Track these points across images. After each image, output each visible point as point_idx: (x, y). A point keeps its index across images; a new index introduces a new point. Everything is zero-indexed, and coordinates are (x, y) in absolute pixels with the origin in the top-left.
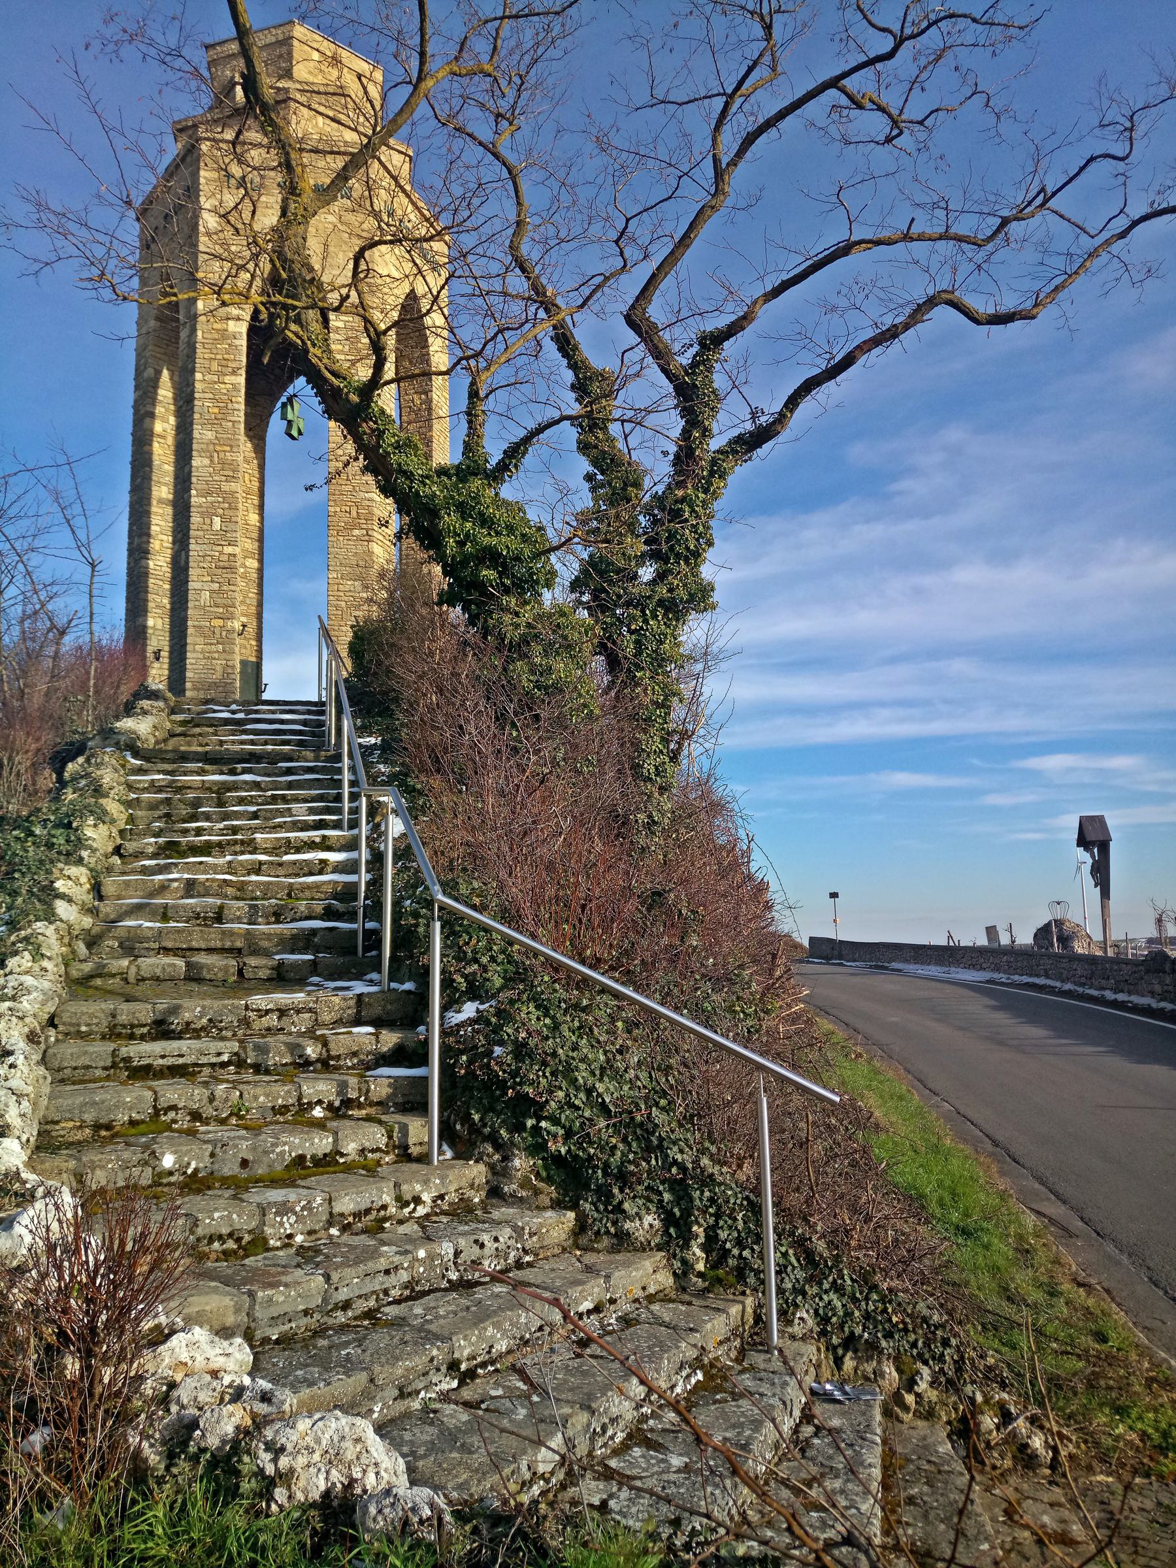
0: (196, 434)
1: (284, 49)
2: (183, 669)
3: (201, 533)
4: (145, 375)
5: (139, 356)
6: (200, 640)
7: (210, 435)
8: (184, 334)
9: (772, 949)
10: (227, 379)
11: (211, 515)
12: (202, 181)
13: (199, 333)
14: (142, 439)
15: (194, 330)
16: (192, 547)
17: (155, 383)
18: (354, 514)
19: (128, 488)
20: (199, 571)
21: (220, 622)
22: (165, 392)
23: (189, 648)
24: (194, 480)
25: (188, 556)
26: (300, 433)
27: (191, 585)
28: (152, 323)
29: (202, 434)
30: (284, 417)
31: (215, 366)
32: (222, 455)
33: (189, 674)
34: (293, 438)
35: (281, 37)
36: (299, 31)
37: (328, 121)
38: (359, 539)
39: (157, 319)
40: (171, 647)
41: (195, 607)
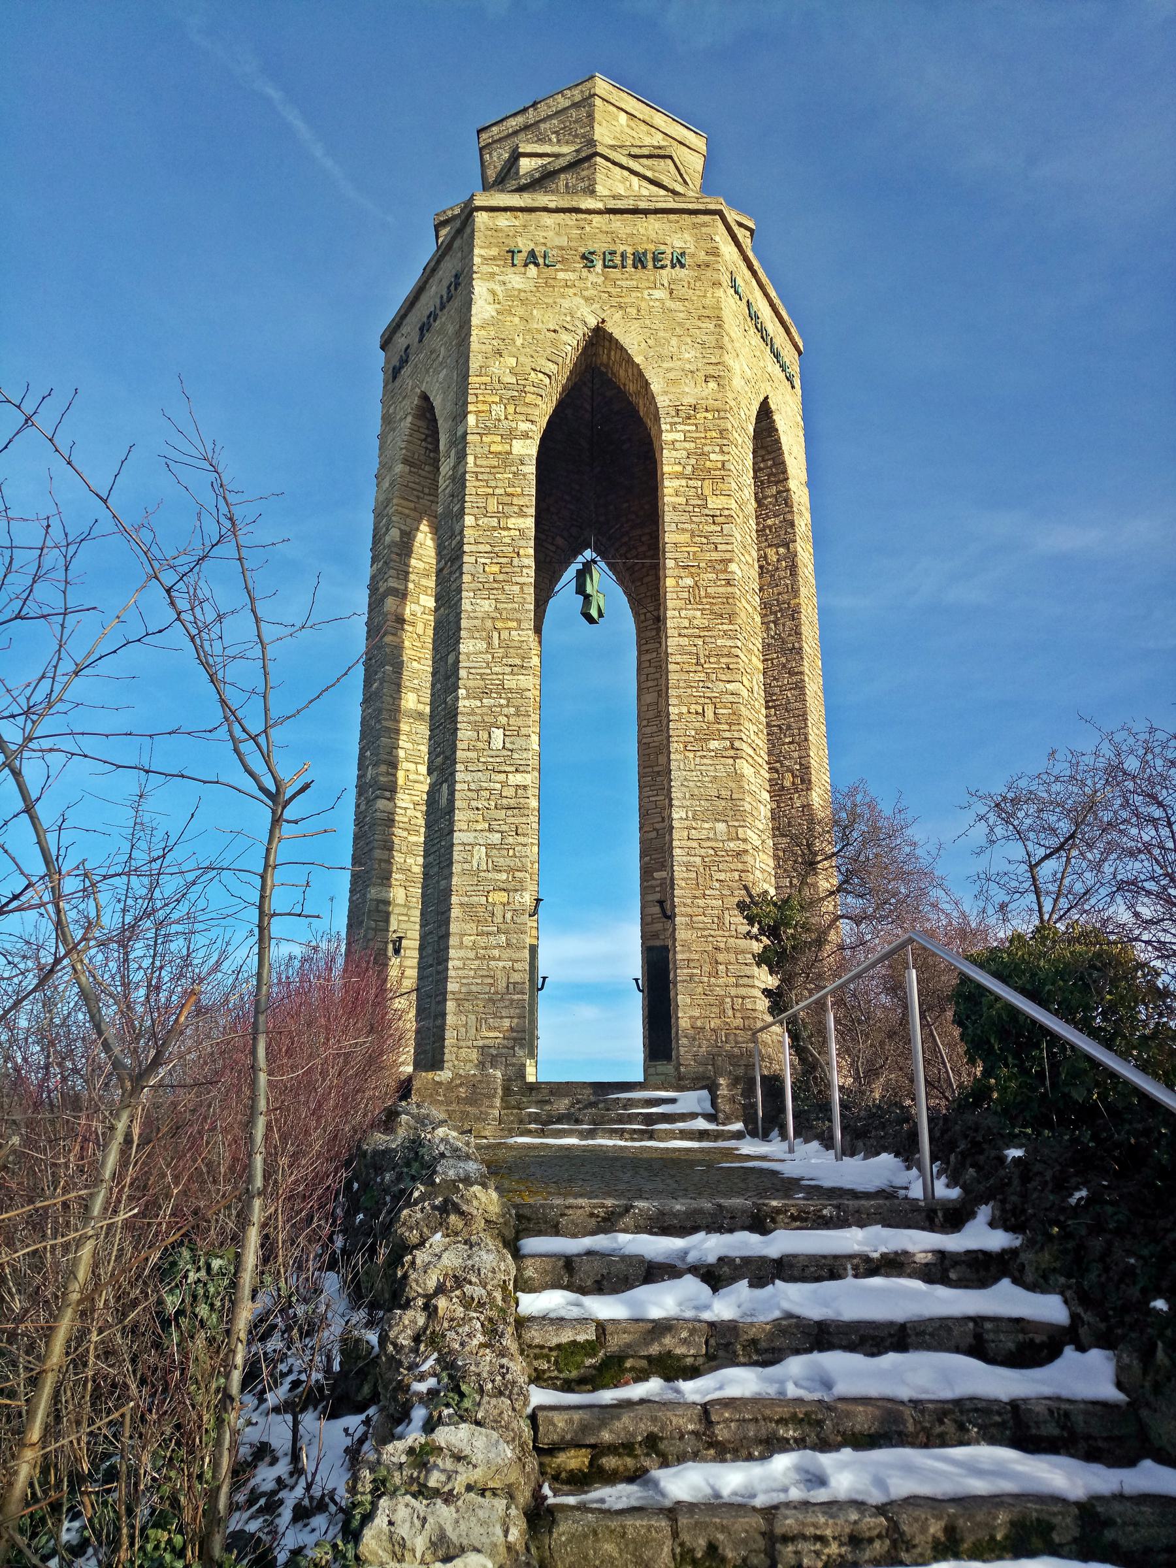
0: (466, 605)
1: (583, 112)
2: (442, 978)
3: (473, 755)
4: (388, 539)
5: (379, 514)
6: (471, 927)
7: (486, 606)
8: (445, 468)
9: (1062, 1293)
10: (511, 522)
11: (489, 727)
12: (477, 260)
13: (470, 459)
14: (384, 627)
15: (462, 456)
16: (459, 776)
17: (405, 547)
18: (710, 715)
19: (360, 698)
20: (471, 815)
21: (502, 897)
22: (425, 541)
23: (453, 941)
24: (463, 673)
25: (452, 792)
26: (601, 615)
27: (458, 837)
28: (399, 468)
29: (475, 605)
30: (581, 589)
31: (493, 505)
32: (504, 635)
33: (452, 986)
34: (591, 620)
35: (578, 98)
36: (602, 86)
37: (645, 184)
38: (718, 755)
39: (405, 461)
40: (423, 938)
41: (464, 872)
